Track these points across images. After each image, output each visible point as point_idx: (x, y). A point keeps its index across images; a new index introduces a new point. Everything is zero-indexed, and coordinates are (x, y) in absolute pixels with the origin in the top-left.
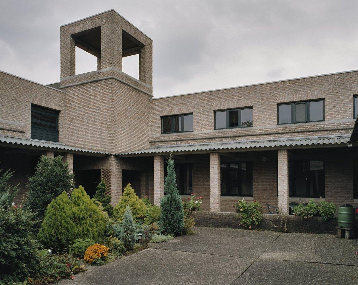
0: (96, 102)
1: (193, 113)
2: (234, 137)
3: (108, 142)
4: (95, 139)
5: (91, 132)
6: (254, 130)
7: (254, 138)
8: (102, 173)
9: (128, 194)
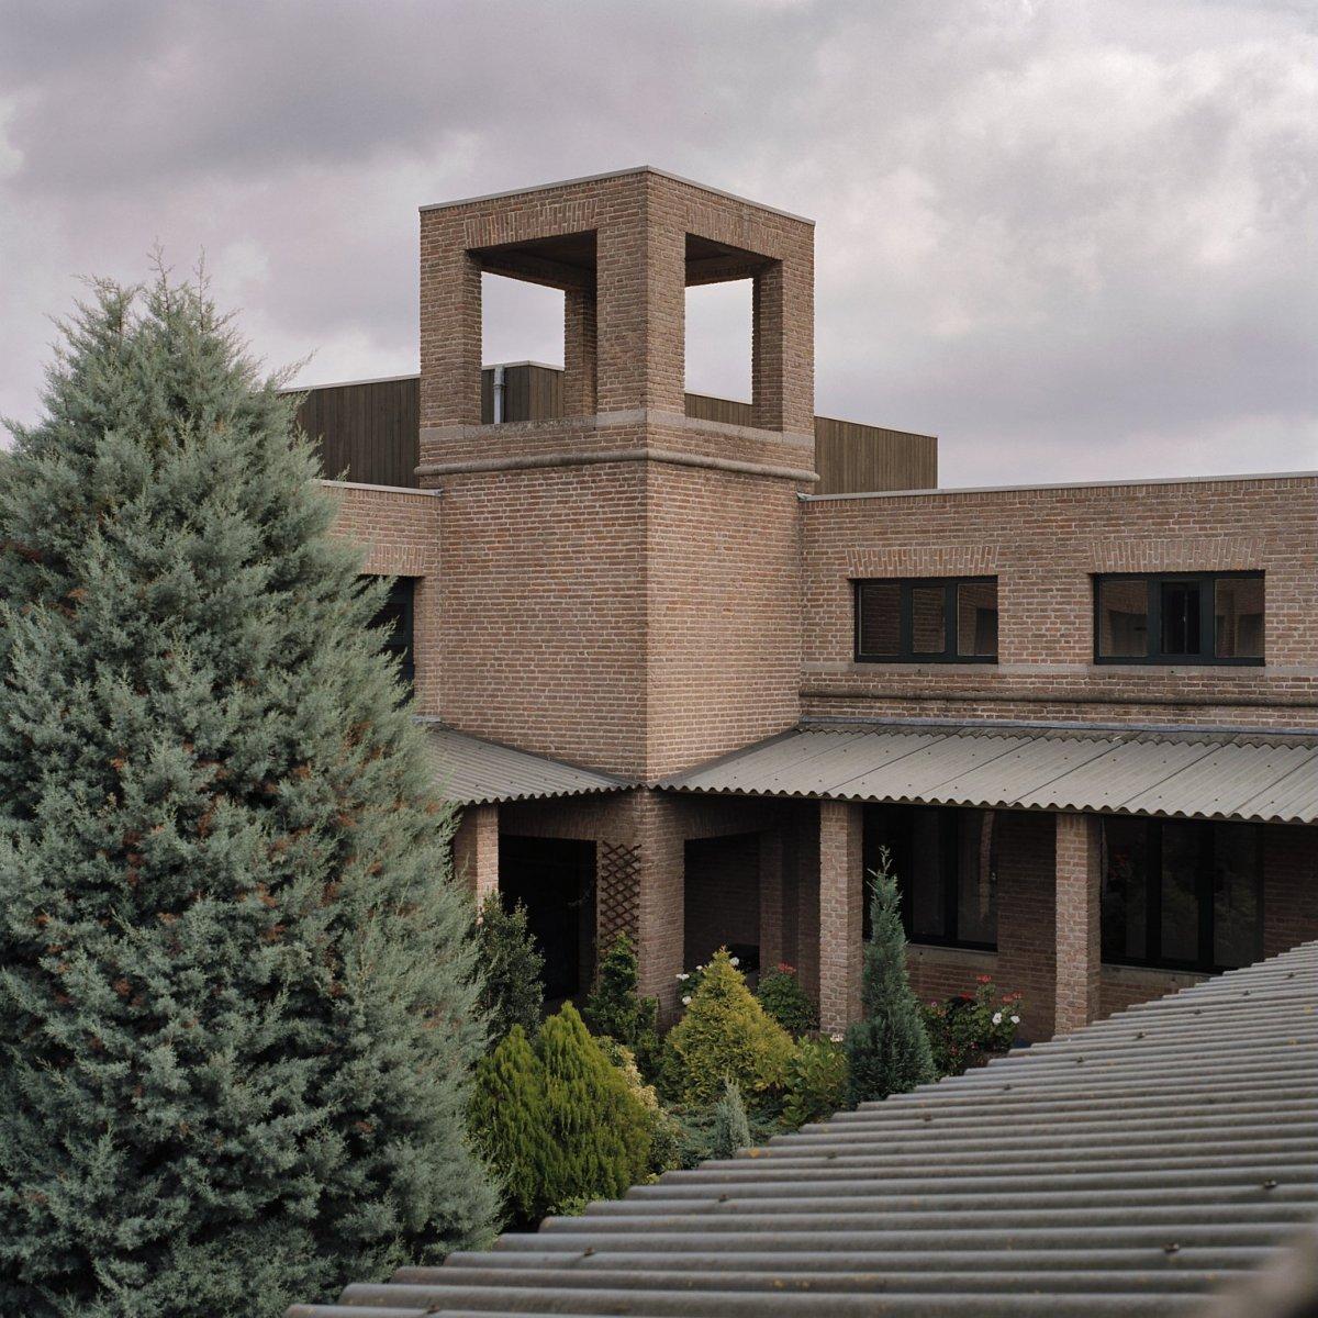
0: (574, 552)
1: (996, 577)
2: (1181, 705)
3: (627, 732)
4: (570, 711)
5: (552, 679)
6: (1272, 679)
7: (1271, 716)
8: (601, 862)
9: (718, 993)
